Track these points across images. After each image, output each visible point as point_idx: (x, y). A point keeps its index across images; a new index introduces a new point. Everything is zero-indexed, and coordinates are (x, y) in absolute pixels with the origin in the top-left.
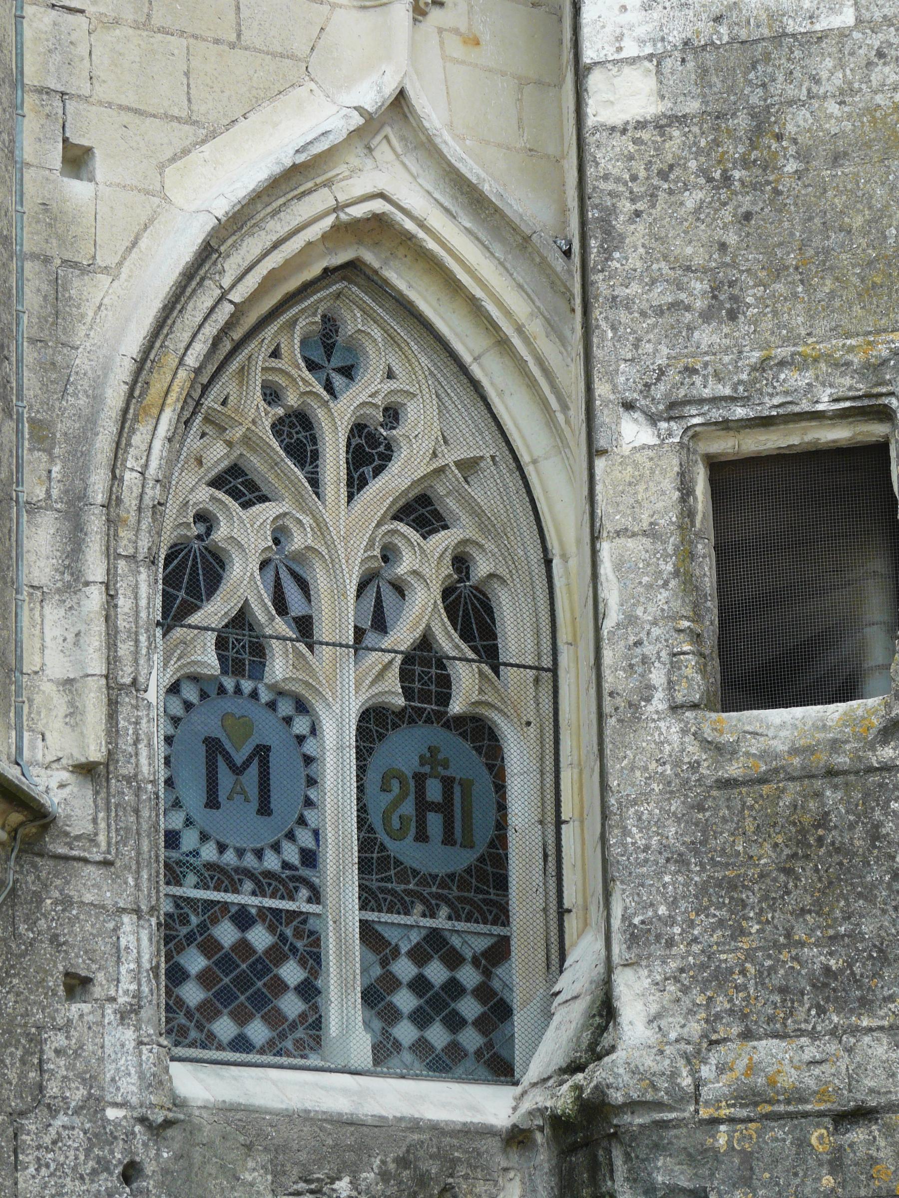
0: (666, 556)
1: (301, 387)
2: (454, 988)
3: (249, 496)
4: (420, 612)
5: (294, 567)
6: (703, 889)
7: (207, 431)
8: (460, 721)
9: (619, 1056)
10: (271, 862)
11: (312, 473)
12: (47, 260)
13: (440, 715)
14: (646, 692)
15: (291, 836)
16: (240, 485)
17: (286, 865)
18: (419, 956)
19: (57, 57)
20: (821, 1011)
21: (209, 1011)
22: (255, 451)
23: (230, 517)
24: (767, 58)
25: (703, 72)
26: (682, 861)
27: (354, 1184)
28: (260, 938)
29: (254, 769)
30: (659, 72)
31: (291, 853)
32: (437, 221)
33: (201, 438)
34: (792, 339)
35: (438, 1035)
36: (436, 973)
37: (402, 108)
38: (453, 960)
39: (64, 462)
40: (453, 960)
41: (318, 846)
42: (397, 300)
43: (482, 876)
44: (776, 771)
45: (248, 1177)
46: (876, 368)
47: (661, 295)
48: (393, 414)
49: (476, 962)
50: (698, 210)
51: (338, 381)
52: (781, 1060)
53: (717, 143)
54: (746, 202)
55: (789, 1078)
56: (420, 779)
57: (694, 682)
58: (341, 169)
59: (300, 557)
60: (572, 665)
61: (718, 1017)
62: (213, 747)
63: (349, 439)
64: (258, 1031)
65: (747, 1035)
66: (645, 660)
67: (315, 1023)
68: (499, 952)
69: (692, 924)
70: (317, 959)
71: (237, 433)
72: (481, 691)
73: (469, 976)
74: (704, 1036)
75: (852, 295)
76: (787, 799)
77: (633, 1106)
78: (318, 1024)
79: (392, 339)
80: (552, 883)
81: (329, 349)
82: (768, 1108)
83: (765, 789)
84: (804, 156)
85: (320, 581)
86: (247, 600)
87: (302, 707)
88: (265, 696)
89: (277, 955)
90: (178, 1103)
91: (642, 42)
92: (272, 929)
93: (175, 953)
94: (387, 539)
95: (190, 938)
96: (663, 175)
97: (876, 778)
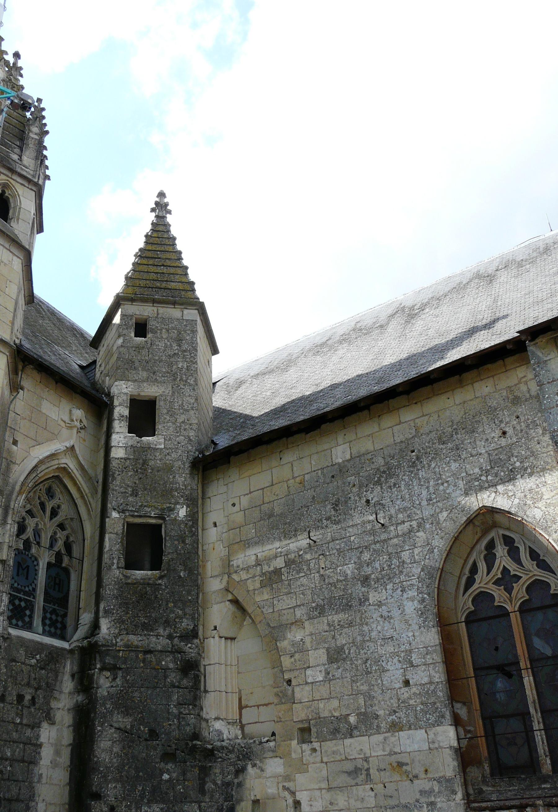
0: (119, 539)
1: (44, 498)
2: (57, 621)
4: (60, 545)
6: (121, 604)
9: (100, 635)
10: (27, 589)
12: (7, 460)
14: (113, 564)
16: (30, 513)
17: (29, 590)
19: (14, 422)
20: (143, 630)
23: (29, 519)
24: (147, 451)
25: (134, 451)
26: (117, 598)
27: (40, 656)
28: (23, 604)
29: (26, 570)
30: (126, 450)
31: (31, 588)
32: (75, 471)
34: (147, 502)
35: (53, 630)
36: (54, 617)
38: (57, 615)
39: (5, 499)
44: (138, 582)
45: (21, 652)
46: (163, 509)
47: (122, 490)
48: (59, 507)
49: (61, 616)
50: (131, 476)
52: (134, 639)
53: (136, 464)
54: (141, 476)
55: (136, 643)
56: (55, 578)
57: (122, 563)
58: (60, 457)
61: (122, 629)
64: (20, 623)
65: (127, 634)
66: (113, 558)
68: (65, 615)
69: (118, 610)
73: (60, 619)
74: (118, 633)
75: (159, 495)
76: (139, 588)
77: (103, 645)
80: (78, 603)
82: (131, 649)
83: (135, 586)
84: (152, 469)
85: (43, 535)
87: (36, 559)
88: (30, 556)
89: (26, 608)
90: (9, 634)
91: (123, 444)
92: (25, 603)
96: (125, 468)
97: (157, 586)
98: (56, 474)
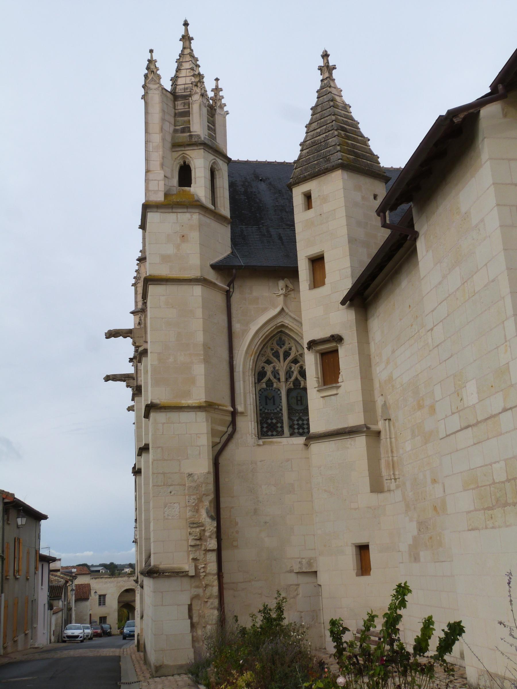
4: (295, 374)
8: (302, 388)
10: (275, 411)
16: (268, 362)
18: (298, 420)
21: (267, 431)
31: (278, 409)
35: (301, 431)
36: (300, 422)
40: (303, 420)
42: (343, 433)
48: (290, 349)
51: (282, 346)
59: (278, 370)
62: (266, 397)
67: (283, 432)
70: (283, 423)
78: (283, 431)
85: (280, 373)
87: (279, 390)
88: (274, 389)
89: (277, 423)
98: (279, 330)
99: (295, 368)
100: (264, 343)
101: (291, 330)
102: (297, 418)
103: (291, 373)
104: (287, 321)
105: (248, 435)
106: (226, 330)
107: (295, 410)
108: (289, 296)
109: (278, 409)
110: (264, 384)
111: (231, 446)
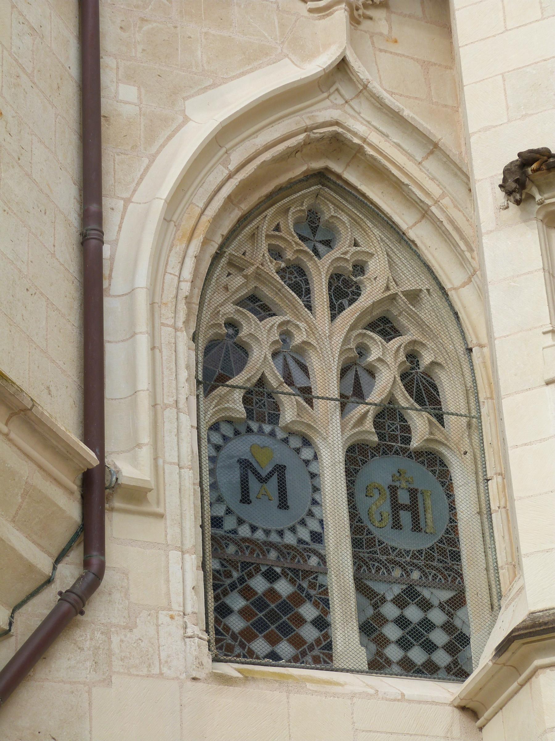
1: (294, 248)
3: (263, 314)
4: (385, 383)
5: (297, 357)
7: (231, 272)
10: (290, 539)
11: (307, 301)
13: (404, 451)
15: (303, 523)
17: (300, 541)
21: (248, 635)
22: (264, 283)
28: (284, 588)
29: (274, 480)
31: (304, 534)
33: (227, 276)
35: (417, 655)
36: (413, 613)
37: (348, 75)
38: (425, 605)
40: (425, 605)
41: (323, 528)
43: (442, 552)
48: (360, 268)
49: (441, 607)
60: (491, 411)
62: (245, 465)
63: (330, 282)
68: (458, 601)
70: (327, 602)
71: (250, 270)
72: (431, 433)
73: (437, 617)
78: (329, 647)
79: (355, 221)
81: (314, 230)
85: (314, 362)
86: (263, 374)
87: (307, 442)
88: (281, 435)
89: (298, 599)
92: (292, 581)
93: (222, 596)
94: (359, 340)
95: (233, 587)
98: (317, 165)
99: (387, 358)
100: (245, 207)
101: (378, 171)
102: (397, 590)
103: (364, 378)
104: (363, 126)
105: (163, 617)
106: (69, 92)
107: (385, 551)
108: (366, 25)
109: (304, 534)
110: (238, 395)
111: (68, 663)
